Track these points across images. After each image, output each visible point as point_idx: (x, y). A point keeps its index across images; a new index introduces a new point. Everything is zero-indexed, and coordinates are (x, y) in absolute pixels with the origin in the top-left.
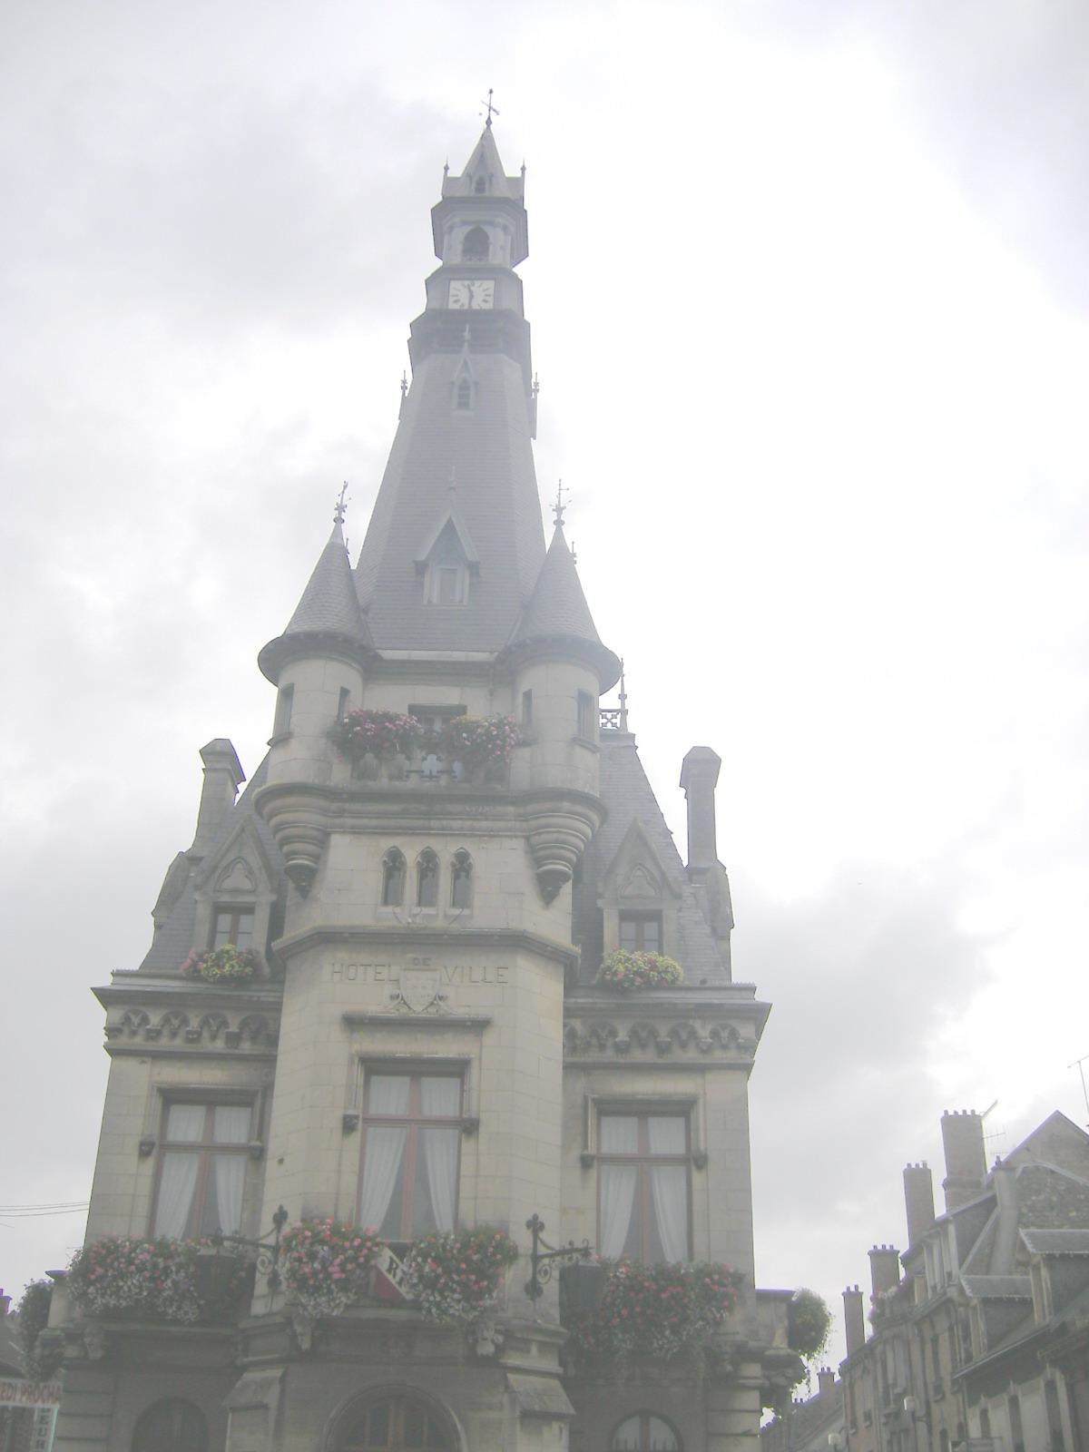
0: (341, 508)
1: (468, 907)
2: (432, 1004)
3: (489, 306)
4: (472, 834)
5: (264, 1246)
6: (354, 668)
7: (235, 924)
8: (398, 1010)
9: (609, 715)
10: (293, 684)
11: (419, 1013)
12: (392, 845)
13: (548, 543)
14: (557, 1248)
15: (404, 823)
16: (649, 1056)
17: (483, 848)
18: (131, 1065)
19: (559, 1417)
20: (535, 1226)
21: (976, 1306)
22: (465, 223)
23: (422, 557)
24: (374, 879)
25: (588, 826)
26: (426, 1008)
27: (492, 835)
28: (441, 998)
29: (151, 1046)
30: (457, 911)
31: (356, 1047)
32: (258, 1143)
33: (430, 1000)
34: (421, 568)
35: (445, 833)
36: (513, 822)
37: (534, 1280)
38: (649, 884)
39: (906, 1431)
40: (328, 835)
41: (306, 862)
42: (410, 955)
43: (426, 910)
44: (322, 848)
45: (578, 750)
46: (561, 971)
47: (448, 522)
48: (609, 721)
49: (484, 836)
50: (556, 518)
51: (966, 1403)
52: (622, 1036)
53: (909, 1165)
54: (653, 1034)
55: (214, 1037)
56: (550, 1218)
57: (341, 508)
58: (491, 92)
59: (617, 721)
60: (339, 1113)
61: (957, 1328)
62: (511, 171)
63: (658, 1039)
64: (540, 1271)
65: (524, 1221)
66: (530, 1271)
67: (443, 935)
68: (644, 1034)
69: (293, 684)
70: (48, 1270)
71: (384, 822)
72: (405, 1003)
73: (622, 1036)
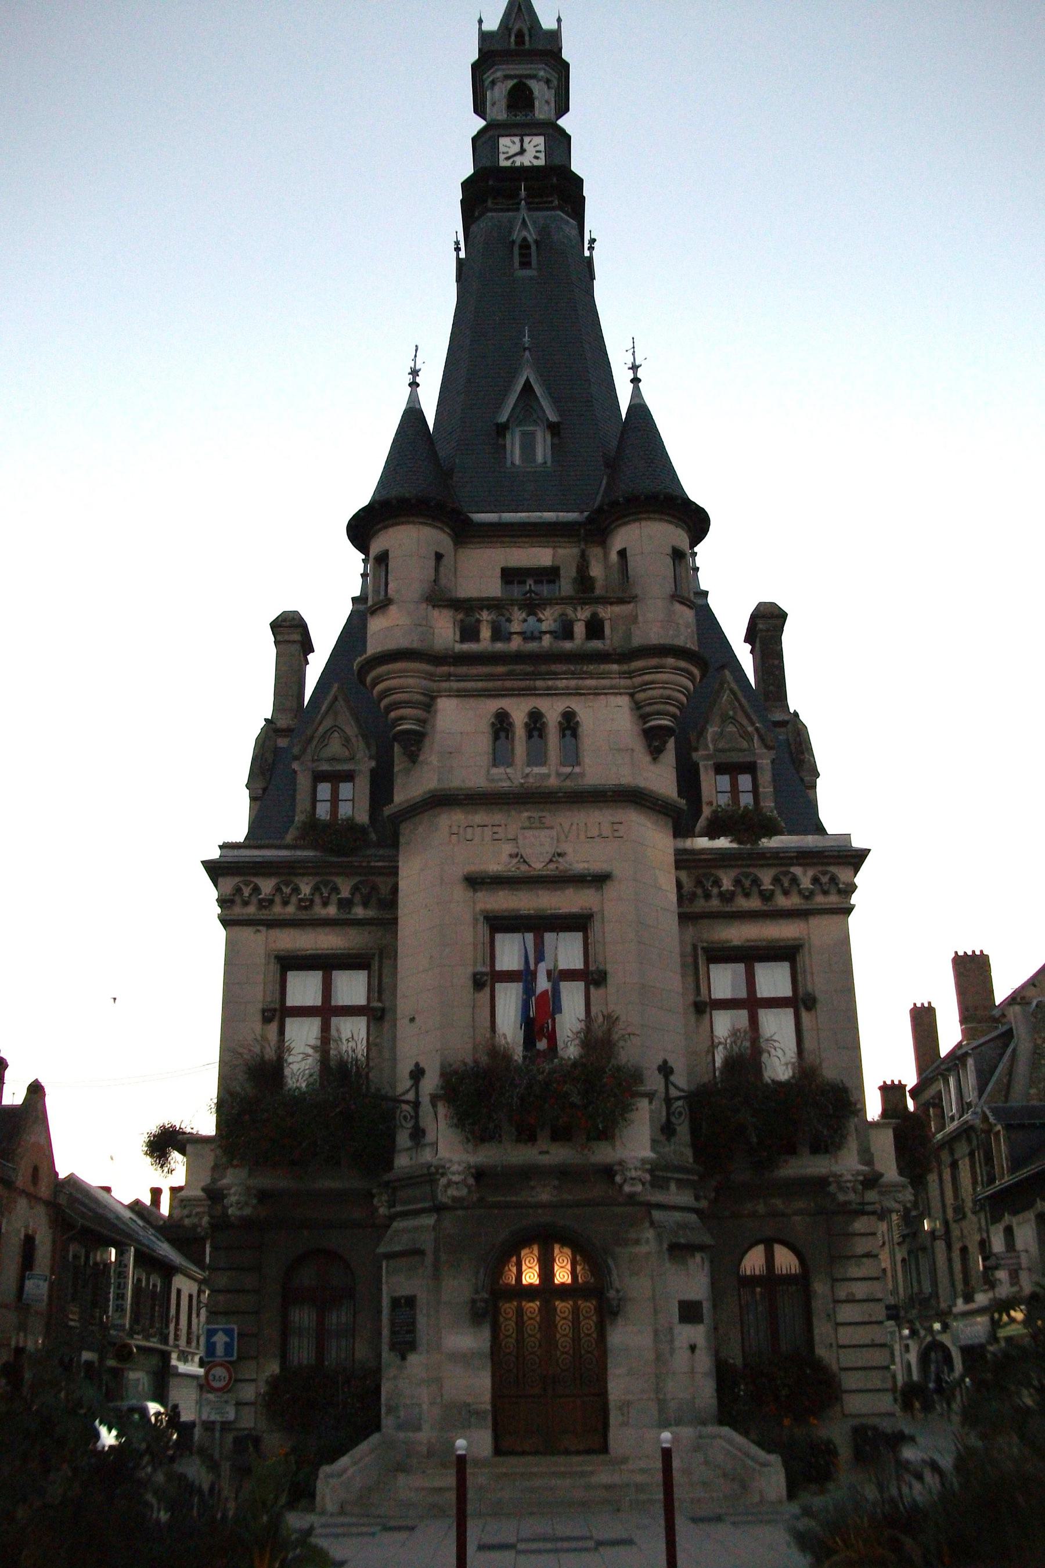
0: (414, 372)
1: (578, 764)
2: (551, 861)
3: (541, 162)
4: (577, 693)
6: (445, 532)
7: (335, 793)
8: (518, 868)
10: (387, 551)
11: (539, 870)
12: (497, 708)
13: (624, 405)
15: (508, 684)
16: (754, 903)
17: (589, 706)
18: (246, 934)
19: (701, 1248)
20: (666, 1070)
21: (999, 1131)
22: (507, 77)
23: (503, 418)
24: (483, 743)
25: (688, 678)
27: (596, 693)
28: (559, 855)
29: (264, 915)
30: (568, 770)
31: (480, 906)
32: (380, 1005)
33: (550, 858)
34: (502, 430)
35: (551, 693)
36: (618, 680)
38: (741, 736)
39: (924, 1249)
40: (433, 698)
41: (414, 727)
42: (526, 814)
43: (536, 770)
44: (429, 712)
45: (678, 607)
46: (670, 824)
47: (525, 385)
49: (589, 694)
50: (632, 376)
51: (989, 1221)
52: (727, 884)
53: (915, 1004)
54: (756, 882)
55: (325, 904)
56: (678, 1064)
57: (414, 372)
60: (470, 970)
61: (979, 1152)
62: (547, 23)
63: (762, 888)
64: (674, 1113)
65: (655, 1067)
66: (664, 1113)
67: (557, 793)
68: (747, 883)
69: (387, 551)
71: (490, 685)
72: (525, 861)
73: (727, 884)
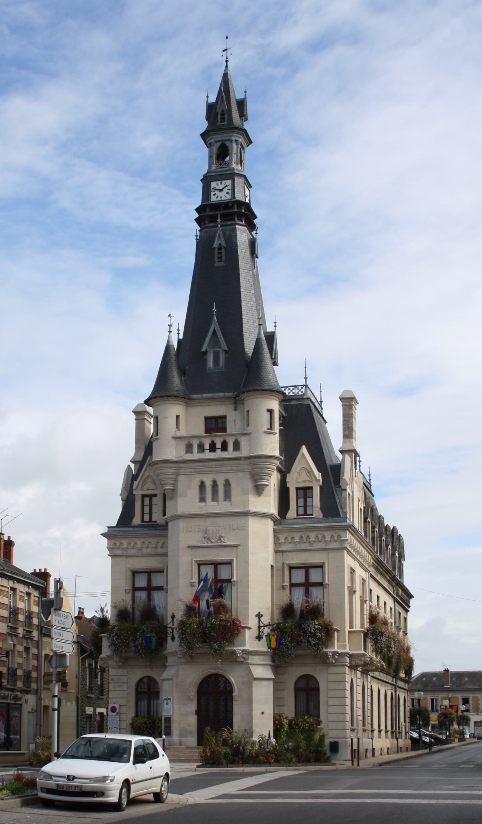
2: (219, 539)
5: (169, 627)
9: (300, 388)
14: (266, 624)
22: (216, 142)
23: (203, 349)
24: (195, 492)
26: (217, 541)
37: (259, 635)
48: (300, 390)
58: (227, 38)
59: (303, 390)
70: (101, 533)
